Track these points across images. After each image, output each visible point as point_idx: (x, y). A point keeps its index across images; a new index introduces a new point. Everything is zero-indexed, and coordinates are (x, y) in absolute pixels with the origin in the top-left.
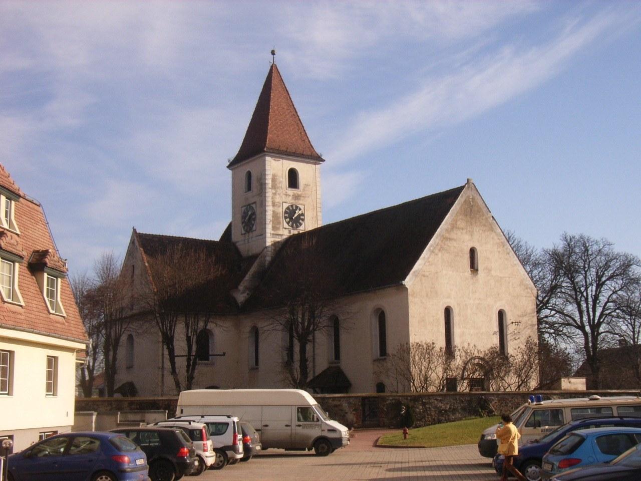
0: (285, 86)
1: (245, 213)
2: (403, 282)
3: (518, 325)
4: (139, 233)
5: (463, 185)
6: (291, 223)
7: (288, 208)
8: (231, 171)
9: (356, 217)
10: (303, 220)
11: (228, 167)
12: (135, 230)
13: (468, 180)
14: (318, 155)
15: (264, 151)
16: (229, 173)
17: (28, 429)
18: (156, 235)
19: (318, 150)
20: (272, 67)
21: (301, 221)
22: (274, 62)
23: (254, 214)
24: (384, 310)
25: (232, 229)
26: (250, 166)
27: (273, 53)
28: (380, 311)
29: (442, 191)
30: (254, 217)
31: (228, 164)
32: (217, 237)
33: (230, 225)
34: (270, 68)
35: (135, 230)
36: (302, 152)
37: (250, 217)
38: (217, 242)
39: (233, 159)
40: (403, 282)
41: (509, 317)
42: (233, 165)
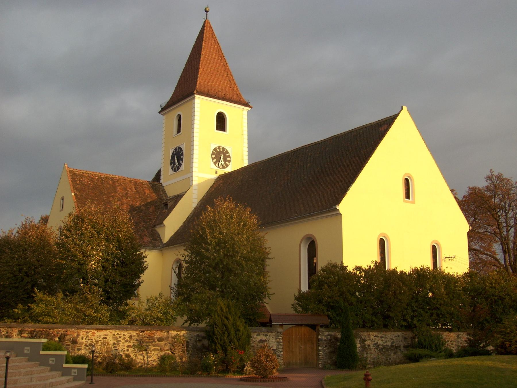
2: (338, 207)
20: (205, 22)
26: (180, 110)
34: (203, 23)
40: (338, 207)
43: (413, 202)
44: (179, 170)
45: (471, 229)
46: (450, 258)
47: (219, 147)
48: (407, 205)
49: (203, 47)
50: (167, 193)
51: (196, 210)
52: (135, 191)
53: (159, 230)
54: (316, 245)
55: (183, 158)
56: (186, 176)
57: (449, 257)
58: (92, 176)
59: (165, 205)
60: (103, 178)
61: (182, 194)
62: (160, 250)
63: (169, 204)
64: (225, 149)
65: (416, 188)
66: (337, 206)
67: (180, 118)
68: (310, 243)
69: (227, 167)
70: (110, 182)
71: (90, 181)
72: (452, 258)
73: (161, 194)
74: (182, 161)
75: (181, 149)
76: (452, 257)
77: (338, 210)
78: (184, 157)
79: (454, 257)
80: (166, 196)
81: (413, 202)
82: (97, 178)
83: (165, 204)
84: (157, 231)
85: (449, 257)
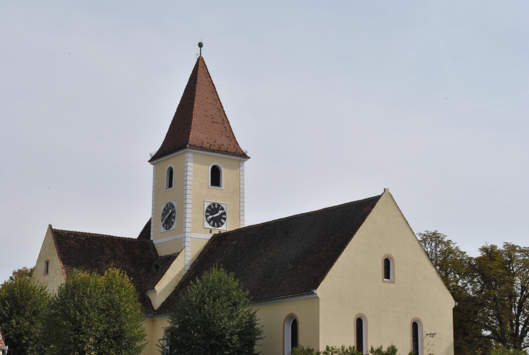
0: (211, 80)
1: (166, 211)
3: (432, 336)
4: (55, 229)
5: (380, 194)
6: (212, 222)
7: (209, 207)
8: (152, 166)
9: (277, 220)
10: (225, 219)
11: (150, 161)
12: (50, 226)
13: (385, 189)
14: (243, 151)
15: (187, 147)
16: (151, 167)
17: (411, 228)
18: (72, 231)
19: (244, 146)
20: (198, 59)
21: (222, 220)
22: (200, 55)
23: (174, 212)
24: (296, 319)
25: (152, 229)
26: (171, 161)
27: (200, 45)
28: (294, 319)
29: (360, 199)
30: (174, 215)
31: (150, 158)
32: (135, 235)
33: (151, 218)
34: (196, 60)
35: (50, 226)
36: (226, 149)
37: (171, 214)
38: (135, 239)
39: (155, 153)
40: (315, 292)
41: (424, 330)
42: (154, 159)
43: (393, 282)
44: (171, 229)
45: (457, 305)
46: (431, 335)
47: (214, 204)
48: (387, 285)
49: (193, 122)
50: (158, 252)
51: (189, 274)
52: (124, 251)
53: (150, 295)
54: (298, 324)
55: (175, 216)
56: (180, 236)
57: (430, 334)
58: (78, 237)
59: (156, 267)
60: (90, 238)
61: (174, 255)
62: (151, 317)
63: (160, 266)
64: (220, 205)
65: (396, 269)
66: (315, 290)
67: (171, 172)
68: (292, 323)
69: (222, 225)
70: (98, 243)
71: (76, 243)
72: (432, 335)
73: (151, 254)
74: (174, 219)
75: (173, 205)
76: (432, 334)
77: (316, 294)
78: (177, 215)
79: (434, 334)
80: (157, 255)
81: (393, 282)
82: (83, 238)
83: (156, 266)
84: (148, 297)
85: (430, 334)
